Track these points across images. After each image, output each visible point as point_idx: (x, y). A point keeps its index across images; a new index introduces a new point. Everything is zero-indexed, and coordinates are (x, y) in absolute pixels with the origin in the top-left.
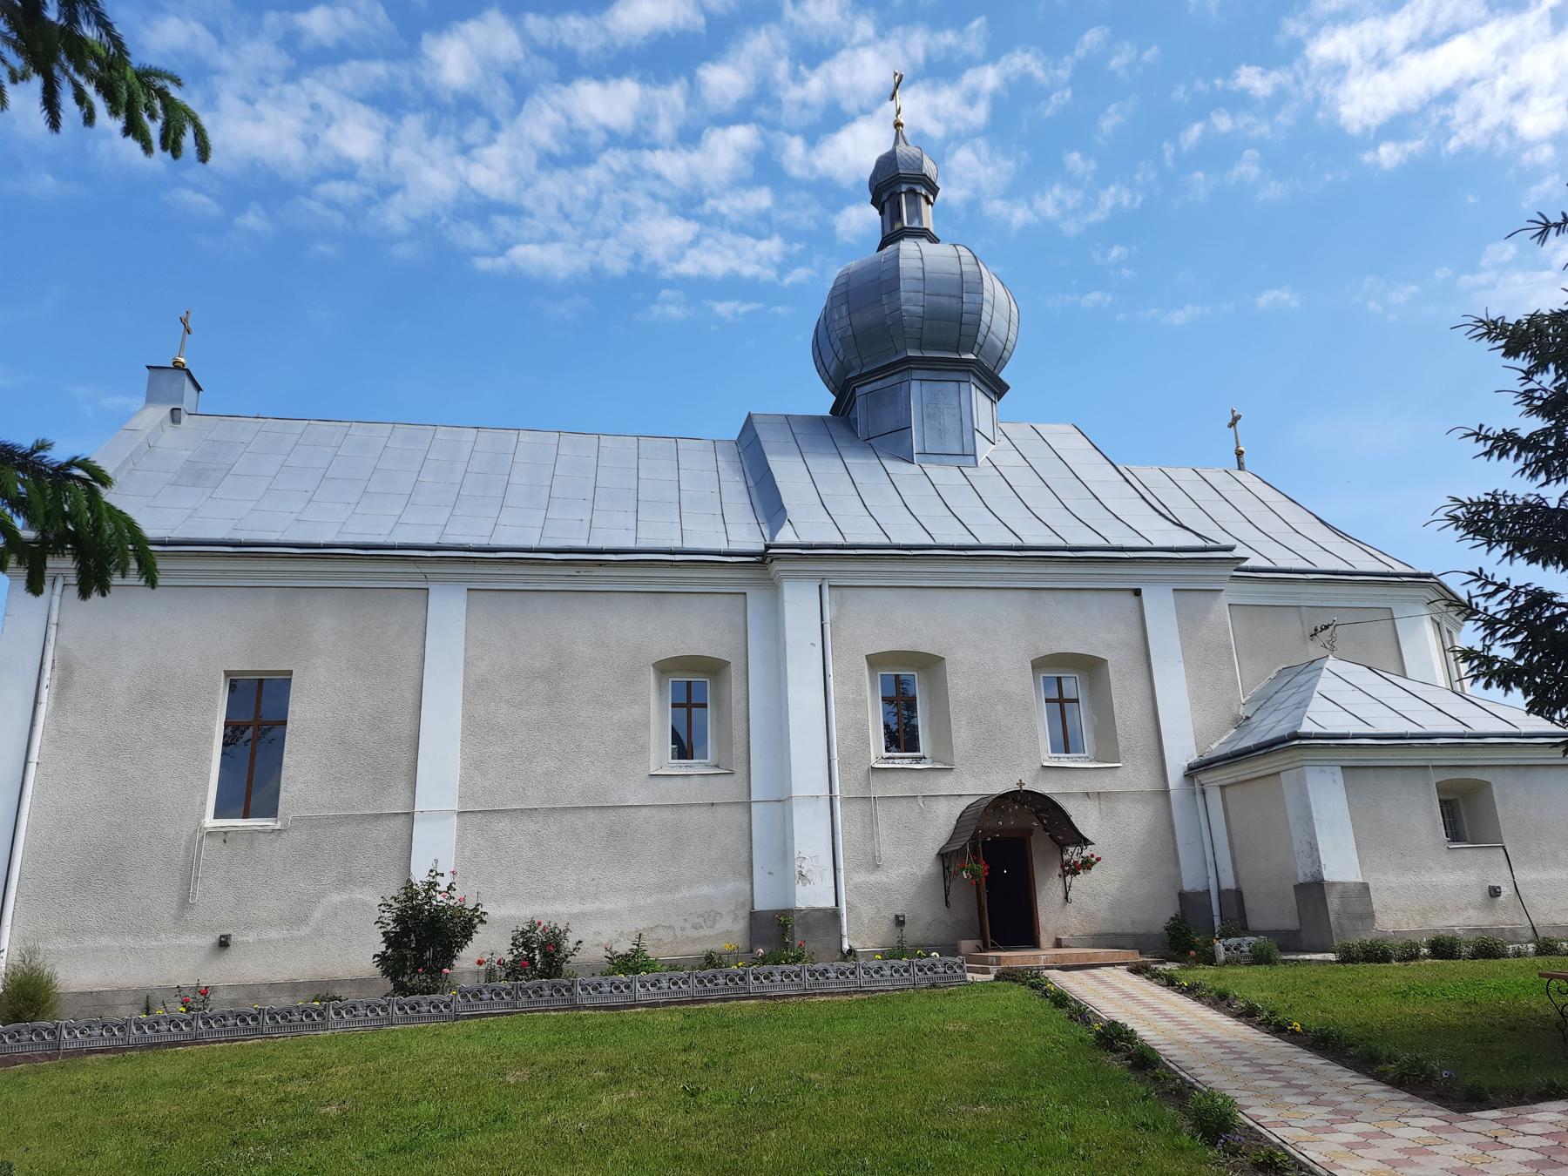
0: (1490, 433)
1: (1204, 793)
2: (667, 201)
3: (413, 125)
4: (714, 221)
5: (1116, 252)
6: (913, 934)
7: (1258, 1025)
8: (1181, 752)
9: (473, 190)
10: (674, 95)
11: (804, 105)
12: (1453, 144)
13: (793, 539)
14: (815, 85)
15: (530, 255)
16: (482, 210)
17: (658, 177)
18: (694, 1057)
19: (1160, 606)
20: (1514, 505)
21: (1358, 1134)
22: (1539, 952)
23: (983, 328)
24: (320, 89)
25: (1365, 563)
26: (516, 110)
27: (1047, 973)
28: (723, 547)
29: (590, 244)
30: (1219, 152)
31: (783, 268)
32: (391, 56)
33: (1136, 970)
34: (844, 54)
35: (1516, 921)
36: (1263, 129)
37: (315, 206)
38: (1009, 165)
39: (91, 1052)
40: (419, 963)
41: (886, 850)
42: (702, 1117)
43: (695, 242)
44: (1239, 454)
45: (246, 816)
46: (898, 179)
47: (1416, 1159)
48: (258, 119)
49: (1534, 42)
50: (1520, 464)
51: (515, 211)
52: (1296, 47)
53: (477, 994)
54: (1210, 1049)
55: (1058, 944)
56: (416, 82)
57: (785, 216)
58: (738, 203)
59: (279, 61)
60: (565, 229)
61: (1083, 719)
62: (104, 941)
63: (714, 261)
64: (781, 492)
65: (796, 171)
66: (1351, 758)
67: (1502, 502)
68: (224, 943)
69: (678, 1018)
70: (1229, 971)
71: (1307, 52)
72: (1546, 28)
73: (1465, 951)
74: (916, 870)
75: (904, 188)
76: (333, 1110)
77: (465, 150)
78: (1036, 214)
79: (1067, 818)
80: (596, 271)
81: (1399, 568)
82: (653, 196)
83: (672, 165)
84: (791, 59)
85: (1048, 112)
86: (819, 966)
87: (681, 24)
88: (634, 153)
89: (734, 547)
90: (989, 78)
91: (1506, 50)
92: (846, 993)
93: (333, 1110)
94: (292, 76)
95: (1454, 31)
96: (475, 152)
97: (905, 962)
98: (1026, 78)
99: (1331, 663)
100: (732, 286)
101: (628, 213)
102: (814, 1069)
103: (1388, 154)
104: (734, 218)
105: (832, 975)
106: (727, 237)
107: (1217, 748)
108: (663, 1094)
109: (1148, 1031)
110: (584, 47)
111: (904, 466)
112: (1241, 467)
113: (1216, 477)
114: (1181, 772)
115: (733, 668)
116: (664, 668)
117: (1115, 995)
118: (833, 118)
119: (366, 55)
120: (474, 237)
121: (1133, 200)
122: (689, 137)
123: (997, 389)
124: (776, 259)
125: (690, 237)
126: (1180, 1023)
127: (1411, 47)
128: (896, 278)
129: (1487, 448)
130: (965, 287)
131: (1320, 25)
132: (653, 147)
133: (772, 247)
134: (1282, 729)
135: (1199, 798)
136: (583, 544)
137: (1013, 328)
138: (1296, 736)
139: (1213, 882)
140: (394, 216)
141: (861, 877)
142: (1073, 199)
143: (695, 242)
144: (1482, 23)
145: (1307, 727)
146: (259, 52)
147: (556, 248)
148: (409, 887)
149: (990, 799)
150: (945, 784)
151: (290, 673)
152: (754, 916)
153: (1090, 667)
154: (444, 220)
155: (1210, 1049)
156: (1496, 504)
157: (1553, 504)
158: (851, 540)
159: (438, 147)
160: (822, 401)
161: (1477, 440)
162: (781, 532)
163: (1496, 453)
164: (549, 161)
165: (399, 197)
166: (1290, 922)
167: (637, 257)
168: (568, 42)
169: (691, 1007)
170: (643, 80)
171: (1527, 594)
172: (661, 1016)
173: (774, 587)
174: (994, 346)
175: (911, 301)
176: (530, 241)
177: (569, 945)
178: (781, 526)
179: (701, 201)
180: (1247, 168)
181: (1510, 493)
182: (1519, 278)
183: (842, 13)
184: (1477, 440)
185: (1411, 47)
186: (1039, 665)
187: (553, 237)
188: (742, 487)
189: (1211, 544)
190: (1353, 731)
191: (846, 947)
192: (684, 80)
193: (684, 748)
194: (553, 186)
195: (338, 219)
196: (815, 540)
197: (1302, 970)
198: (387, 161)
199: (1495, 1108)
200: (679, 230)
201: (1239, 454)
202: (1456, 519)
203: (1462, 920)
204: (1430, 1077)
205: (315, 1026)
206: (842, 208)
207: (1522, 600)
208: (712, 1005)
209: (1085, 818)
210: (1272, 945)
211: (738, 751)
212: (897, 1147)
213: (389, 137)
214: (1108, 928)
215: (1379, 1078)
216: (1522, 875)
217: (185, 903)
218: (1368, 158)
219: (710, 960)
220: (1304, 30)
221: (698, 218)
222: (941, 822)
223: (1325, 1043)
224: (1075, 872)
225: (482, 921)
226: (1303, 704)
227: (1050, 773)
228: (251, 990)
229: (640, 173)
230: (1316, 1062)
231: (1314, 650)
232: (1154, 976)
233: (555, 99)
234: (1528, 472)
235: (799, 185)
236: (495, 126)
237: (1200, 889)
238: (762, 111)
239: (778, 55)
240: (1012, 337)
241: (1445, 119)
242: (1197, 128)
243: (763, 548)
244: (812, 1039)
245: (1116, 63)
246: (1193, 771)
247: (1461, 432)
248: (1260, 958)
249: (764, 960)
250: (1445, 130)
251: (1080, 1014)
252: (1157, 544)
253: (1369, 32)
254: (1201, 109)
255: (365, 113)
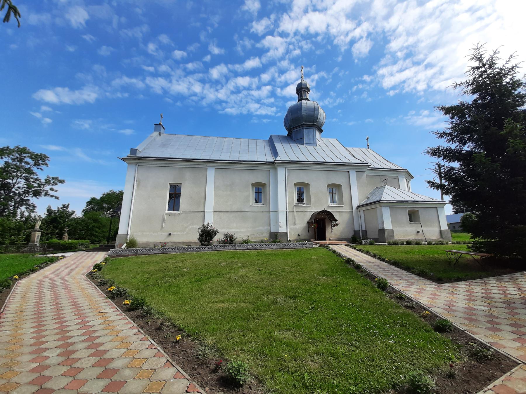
0: (439, 133)
1: (360, 211)
2: (254, 100)
3: (207, 86)
4: (263, 104)
5: (339, 111)
6: (302, 237)
7: (377, 258)
8: (356, 203)
9: (219, 98)
10: (256, 80)
11: (281, 82)
12: (404, 91)
13: (280, 159)
14: (283, 78)
15: (229, 110)
16: (220, 102)
17: (253, 96)
18: (260, 262)
19: (353, 176)
20: (443, 149)
21: (418, 289)
22: (428, 244)
23: (319, 118)
24: (190, 79)
25: (393, 167)
26: (227, 83)
27: (329, 245)
28: (265, 161)
29: (240, 108)
30: (359, 92)
31: (276, 113)
32: (203, 72)
33: (347, 245)
34: (288, 72)
35: (422, 237)
36: (368, 88)
37: (190, 101)
38: (319, 94)
39: (143, 254)
40: (206, 240)
41: (297, 221)
42: (262, 277)
43: (260, 108)
44: (368, 145)
45: (173, 211)
46: (302, 88)
47: (410, 286)
48: (179, 85)
49: (421, 71)
50: (446, 139)
51: (226, 102)
52: (375, 72)
53: (217, 246)
54: (370, 264)
55: (330, 240)
56: (208, 77)
57: (277, 103)
58: (268, 101)
59: (183, 74)
60: (235, 106)
61: (336, 196)
62: (148, 233)
63: (263, 112)
64: (277, 150)
65: (279, 95)
66: (391, 205)
67: (440, 148)
68: (170, 234)
69: (256, 253)
70: (366, 246)
71: (378, 73)
72: (424, 69)
73: (413, 243)
74: (302, 225)
75: (303, 90)
76: (185, 270)
77: (217, 90)
78: (324, 104)
79: (333, 216)
80: (241, 114)
81: (400, 168)
82: (252, 99)
83: (255, 93)
84: (278, 73)
85: (327, 84)
86: (284, 243)
87: (258, 66)
88: (248, 91)
89: (268, 161)
90: (316, 77)
91: (416, 73)
92: (289, 249)
93: (185, 270)
94: (185, 76)
95: (406, 69)
96: (219, 91)
97: (301, 243)
98: (323, 77)
99: (387, 186)
100: (266, 116)
101: (247, 103)
102: (285, 266)
103: (392, 93)
104: (267, 103)
105: (286, 245)
106: (265, 107)
107: (363, 203)
108: (253, 270)
109: (357, 260)
110: (239, 70)
111: (302, 146)
112: (368, 148)
113: (363, 150)
114: (355, 208)
115: (267, 185)
116: (253, 185)
117: (344, 251)
118: (286, 84)
119: (199, 72)
120: (219, 107)
121: (343, 101)
122: (259, 88)
123: (321, 131)
124: (275, 111)
125: (259, 107)
126: (361, 258)
127: (397, 72)
128: (301, 108)
129: (438, 136)
130: (315, 110)
131: (380, 67)
132: (252, 90)
133: (274, 109)
134: (378, 199)
135: (359, 212)
136: (237, 159)
137: (324, 119)
138: (381, 200)
139: (361, 229)
140: (204, 103)
141: (292, 226)
142: (331, 101)
143: (260, 108)
144: (412, 67)
145: (382, 199)
146: (179, 72)
147: (234, 109)
148: (204, 226)
149: (317, 213)
150: (309, 209)
151: (181, 184)
152: (271, 233)
153: (339, 186)
154: (213, 104)
155: (370, 264)
156: (439, 149)
157: (453, 148)
158: (291, 160)
159: (212, 90)
160: (286, 133)
161: (436, 134)
162: (277, 158)
163: (440, 137)
164: (233, 93)
165: (205, 99)
166: (376, 236)
167: (249, 111)
168: (236, 69)
169: (258, 250)
170: (250, 77)
171: (448, 168)
172: (253, 252)
173: (276, 169)
174: (320, 122)
175: (304, 113)
176: (229, 108)
177: (235, 237)
178: (277, 157)
179: (261, 100)
180: (365, 95)
181: (443, 146)
182: (415, 117)
183: (288, 64)
184: (436, 134)
185: (397, 72)
186: (328, 186)
187: (233, 107)
188: (269, 149)
189: (363, 162)
190: (392, 200)
191: (288, 240)
192: (258, 77)
193: (257, 201)
194: (233, 97)
195: (194, 104)
196: (284, 160)
197: (381, 246)
198: (203, 92)
199: (447, 283)
200: (257, 106)
201: (368, 145)
202: (429, 152)
203: (412, 237)
204: (426, 274)
205: (186, 251)
206: (287, 102)
207: (447, 169)
208: (263, 250)
209: (336, 216)
210: (374, 241)
211: (268, 201)
212: (307, 287)
213: (203, 88)
214: (343, 236)
215: (413, 273)
216: (424, 229)
217: (162, 227)
218: (388, 94)
219: (262, 241)
220: (377, 68)
221: (261, 104)
222: (308, 217)
223: (395, 264)
224: (334, 226)
225: (218, 232)
226: (382, 194)
227: (330, 207)
228: (175, 243)
229: (249, 95)
230: (396, 268)
231: (383, 184)
232: (351, 247)
233: (234, 81)
234: (448, 141)
235: (280, 97)
236: (223, 86)
237: (358, 230)
238: (273, 83)
239: (276, 72)
240: (324, 120)
241: (403, 86)
242: (355, 87)
243: (273, 161)
244: (284, 259)
245: (341, 74)
246: (358, 207)
247: (433, 133)
248: (371, 244)
249: (273, 242)
250: (403, 88)
251: (339, 255)
252: (353, 162)
253: (389, 69)
254: (357, 83)
255: (199, 83)
